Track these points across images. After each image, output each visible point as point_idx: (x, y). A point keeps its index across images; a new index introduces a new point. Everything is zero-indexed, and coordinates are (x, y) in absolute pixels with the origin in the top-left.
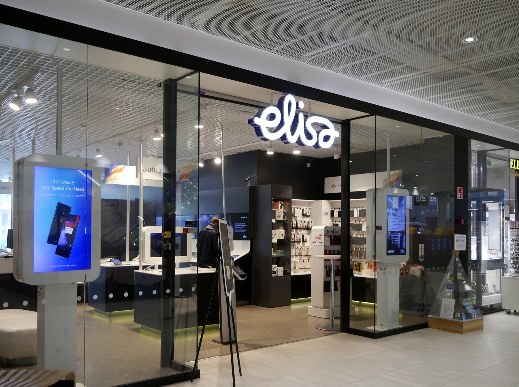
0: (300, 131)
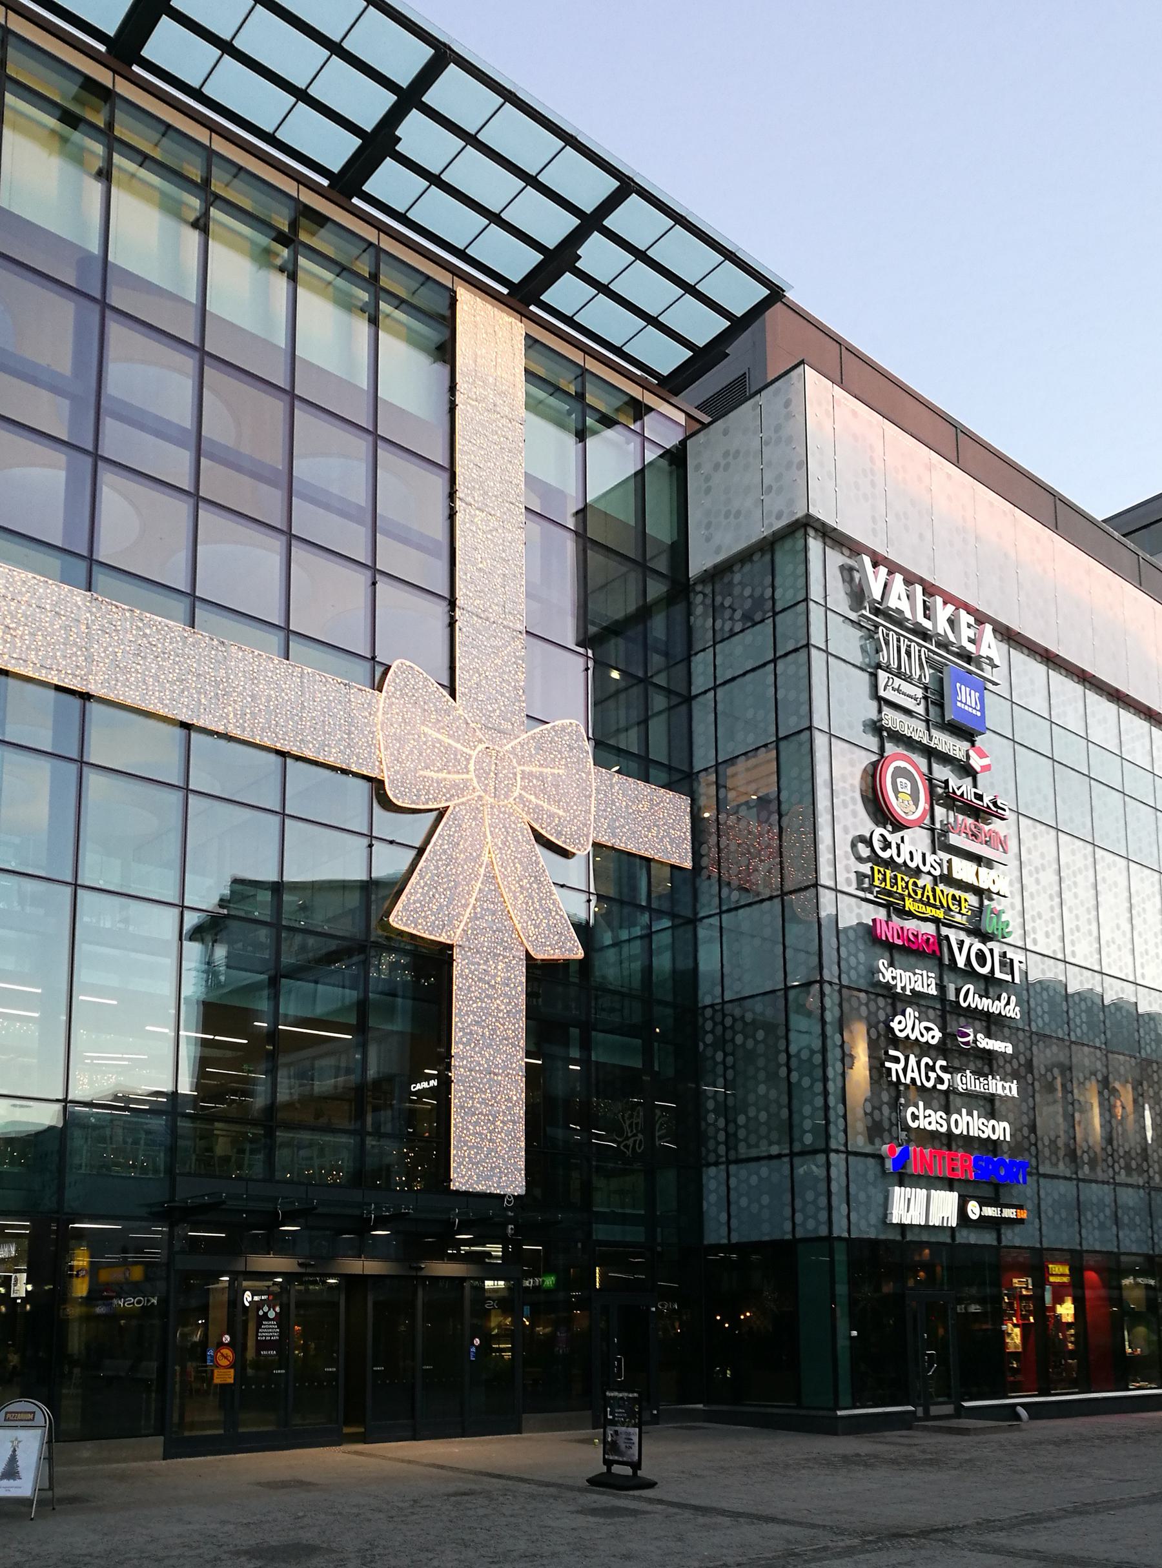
0: (917, 1033)
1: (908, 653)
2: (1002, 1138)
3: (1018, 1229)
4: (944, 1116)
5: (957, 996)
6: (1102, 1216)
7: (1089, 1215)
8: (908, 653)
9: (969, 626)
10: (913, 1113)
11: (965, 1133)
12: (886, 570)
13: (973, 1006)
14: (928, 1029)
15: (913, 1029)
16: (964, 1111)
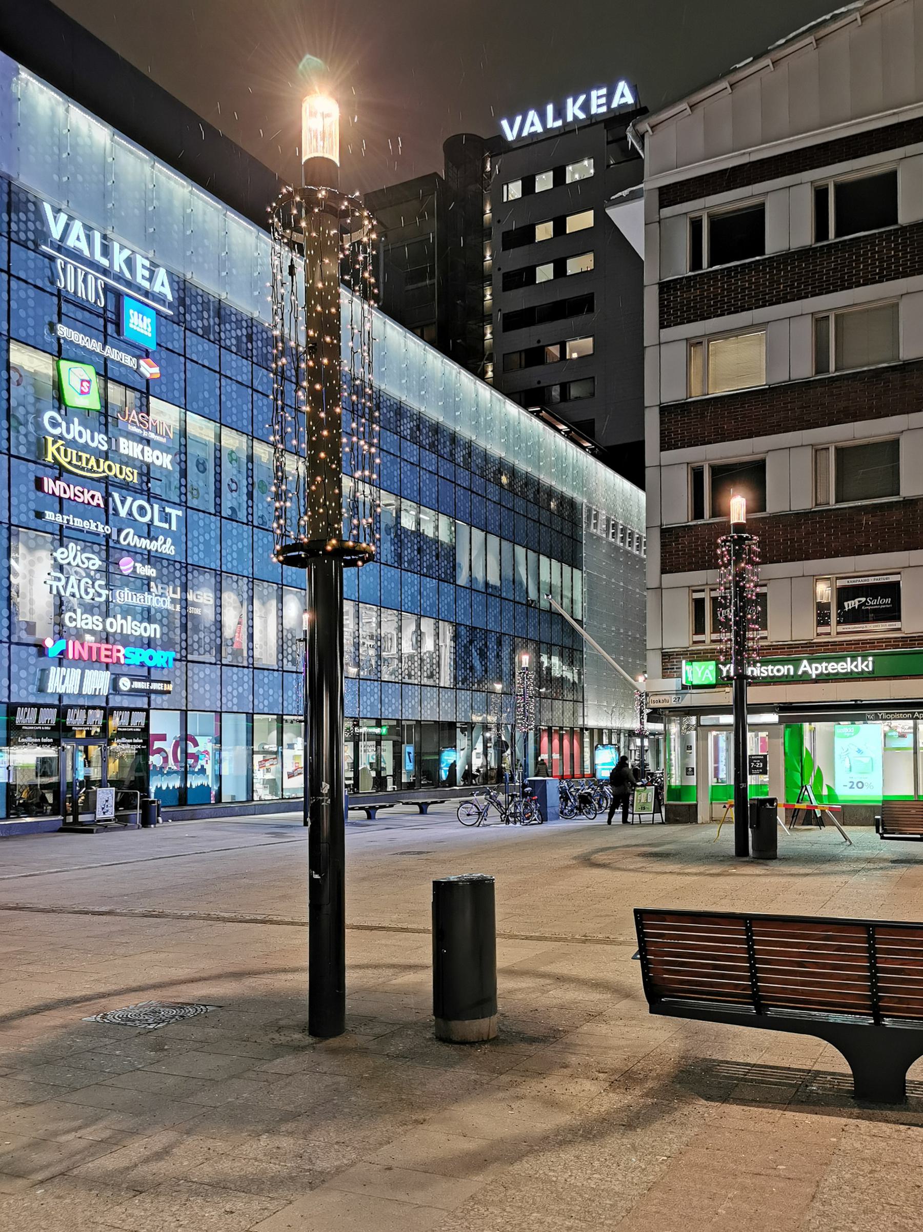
0: (78, 560)
1: (85, 281)
2: (152, 636)
3: (165, 697)
4: (101, 620)
5: (118, 536)
6: (372, 699)
7: (407, 701)
8: (85, 281)
9: (144, 266)
10: (70, 617)
11: (119, 631)
12: (66, 217)
13: (132, 544)
14: (89, 559)
15: (74, 559)
16: (119, 616)
